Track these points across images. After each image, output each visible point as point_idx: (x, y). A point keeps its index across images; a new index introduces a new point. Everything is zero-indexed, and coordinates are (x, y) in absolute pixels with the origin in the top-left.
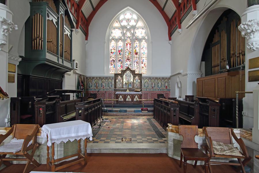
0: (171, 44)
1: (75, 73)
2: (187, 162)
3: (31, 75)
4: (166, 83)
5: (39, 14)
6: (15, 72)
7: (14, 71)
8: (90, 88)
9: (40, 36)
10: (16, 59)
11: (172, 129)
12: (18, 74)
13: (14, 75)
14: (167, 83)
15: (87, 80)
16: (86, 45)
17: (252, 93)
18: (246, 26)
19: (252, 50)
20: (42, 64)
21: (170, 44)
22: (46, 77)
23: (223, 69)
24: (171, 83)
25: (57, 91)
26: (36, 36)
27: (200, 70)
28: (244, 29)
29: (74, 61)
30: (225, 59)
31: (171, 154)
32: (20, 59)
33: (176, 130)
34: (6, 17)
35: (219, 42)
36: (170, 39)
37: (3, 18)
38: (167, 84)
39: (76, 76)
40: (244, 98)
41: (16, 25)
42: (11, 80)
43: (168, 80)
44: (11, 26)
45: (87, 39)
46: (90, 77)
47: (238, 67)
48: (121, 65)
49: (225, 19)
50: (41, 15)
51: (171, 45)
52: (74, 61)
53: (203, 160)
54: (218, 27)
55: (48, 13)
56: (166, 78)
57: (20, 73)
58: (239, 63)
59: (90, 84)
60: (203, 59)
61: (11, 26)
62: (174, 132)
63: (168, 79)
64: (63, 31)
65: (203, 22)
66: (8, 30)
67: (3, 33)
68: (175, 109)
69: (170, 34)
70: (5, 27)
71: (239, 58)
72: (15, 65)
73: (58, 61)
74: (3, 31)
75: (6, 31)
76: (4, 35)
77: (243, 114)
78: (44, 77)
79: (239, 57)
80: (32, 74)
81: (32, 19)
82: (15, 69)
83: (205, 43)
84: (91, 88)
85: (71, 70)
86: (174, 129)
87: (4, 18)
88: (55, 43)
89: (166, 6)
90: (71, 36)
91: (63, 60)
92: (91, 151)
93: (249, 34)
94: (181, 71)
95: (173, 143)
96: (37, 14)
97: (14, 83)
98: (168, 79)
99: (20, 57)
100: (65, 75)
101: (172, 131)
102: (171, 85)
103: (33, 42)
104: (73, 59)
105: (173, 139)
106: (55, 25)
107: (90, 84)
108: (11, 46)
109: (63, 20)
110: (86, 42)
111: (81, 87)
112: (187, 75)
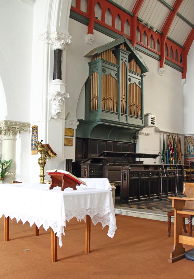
1: (157, 131)
2: (188, 224)
3: (89, 138)
5: (96, 73)
6: (73, 136)
7: (72, 135)
8: (190, 153)
9: (97, 96)
10: (74, 123)
12: (76, 138)
13: (72, 139)
15: (186, 142)
16: (184, 87)
20: (98, 125)
22: (108, 140)
25: (107, 153)
26: (93, 97)
29: (147, 115)
32: (78, 123)
34: (60, 90)
37: (57, 92)
39: (160, 135)
41: (68, 94)
42: (67, 143)
44: (64, 96)
45: (184, 76)
46: (190, 136)
50: (97, 73)
52: (147, 115)
55: (104, 68)
57: (79, 136)
59: (190, 148)
61: (64, 96)
64: (126, 79)
66: (61, 99)
67: (58, 104)
70: (59, 98)
72: (73, 129)
73: (119, 119)
74: (59, 102)
75: (60, 101)
76: (59, 105)
78: (106, 139)
80: (90, 137)
81: (91, 79)
82: (73, 133)
84: (193, 153)
85: (142, 128)
87: (58, 92)
88: (115, 99)
89: (143, 48)
90: (141, 83)
91: (126, 117)
92: (127, 214)
96: (94, 72)
97: (72, 147)
99: (78, 120)
100: (140, 136)
103: (91, 103)
104: (145, 112)
106: (114, 78)
107: (191, 146)
108: (67, 113)
109: (127, 68)
110: (182, 82)
111: (170, 152)
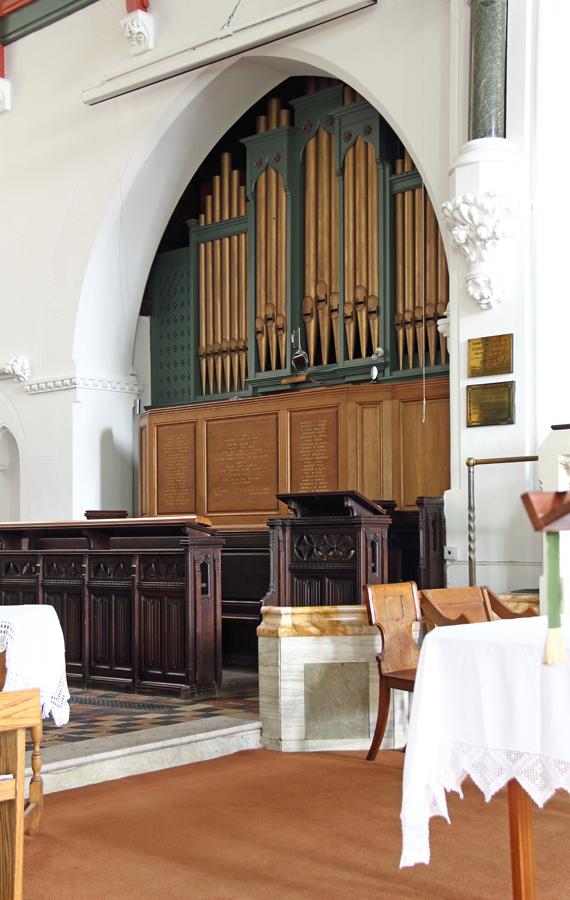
11: (294, 626)
18: (475, 211)
19: (478, 305)
23: (268, 367)
28: (467, 218)
30: (280, 321)
31: (296, 738)
33: (314, 625)
35: (247, 225)
40: (446, 493)
47: (353, 363)
49: (279, 118)
54: (242, 141)
58: (351, 346)
60: (145, 310)
62: (309, 634)
65: (195, 99)
71: (352, 325)
77: (446, 556)
79: (355, 317)
86: (301, 621)
93: (478, 243)
94: (21, 364)
95: (305, 684)
101: (298, 631)
105: (302, 668)
112: (70, 386)
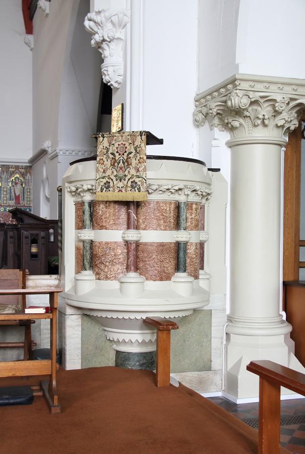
0: (32, 46)
4: (16, 184)
14: (19, 186)
17: (70, 164)
21: (29, 48)
24: (32, 185)
27: (106, 94)
36: (29, 29)
38: (18, 190)
43: (23, 175)
48: (127, 172)
51: (32, 50)
53: (49, 232)
56: (17, 167)
63: (23, 171)
68: (37, 235)
69: (29, 8)
83: (38, 163)
98: (23, 171)
102: (32, 191)
